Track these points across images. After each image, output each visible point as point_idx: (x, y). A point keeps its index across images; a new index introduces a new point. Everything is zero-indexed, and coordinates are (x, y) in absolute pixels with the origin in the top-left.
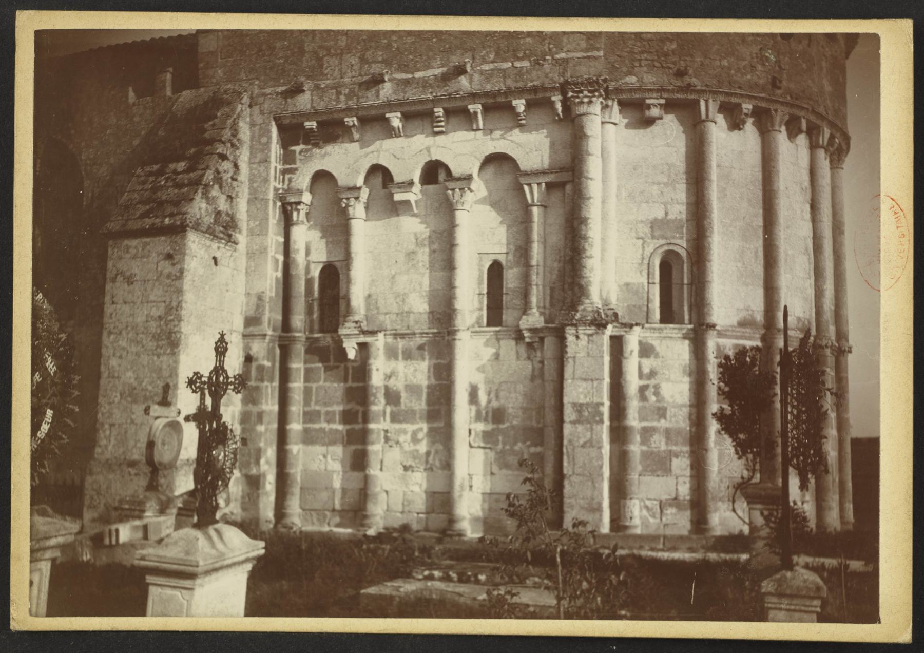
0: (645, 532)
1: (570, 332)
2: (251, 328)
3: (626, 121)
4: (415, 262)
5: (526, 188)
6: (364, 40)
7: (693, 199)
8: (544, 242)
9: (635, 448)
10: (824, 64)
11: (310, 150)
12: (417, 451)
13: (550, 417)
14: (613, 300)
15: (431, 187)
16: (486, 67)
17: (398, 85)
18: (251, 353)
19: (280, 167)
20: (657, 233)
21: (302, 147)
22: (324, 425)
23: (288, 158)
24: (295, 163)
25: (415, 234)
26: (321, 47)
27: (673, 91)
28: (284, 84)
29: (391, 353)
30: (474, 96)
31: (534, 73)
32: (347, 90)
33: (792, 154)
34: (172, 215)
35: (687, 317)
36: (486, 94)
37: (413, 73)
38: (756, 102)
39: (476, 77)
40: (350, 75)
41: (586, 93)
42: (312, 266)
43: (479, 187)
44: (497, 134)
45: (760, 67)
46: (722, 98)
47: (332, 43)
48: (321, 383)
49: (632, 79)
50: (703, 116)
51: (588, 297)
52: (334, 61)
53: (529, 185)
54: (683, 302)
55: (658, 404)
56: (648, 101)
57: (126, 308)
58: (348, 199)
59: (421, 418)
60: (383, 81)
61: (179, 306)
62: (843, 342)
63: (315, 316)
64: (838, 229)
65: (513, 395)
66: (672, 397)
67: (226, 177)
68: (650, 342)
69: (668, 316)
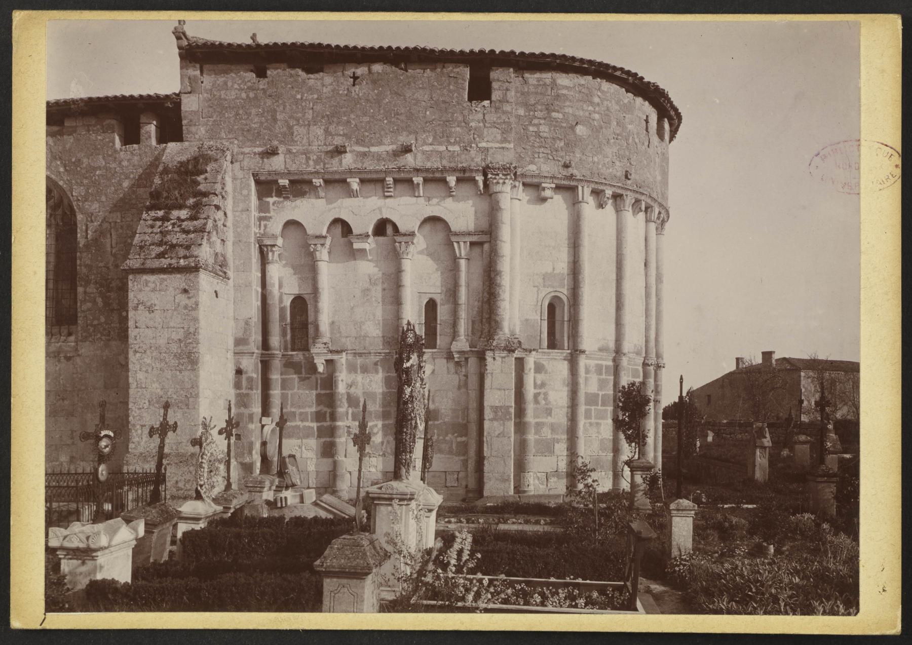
0: (536, 493)
1: (489, 354)
2: (240, 347)
3: (528, 198)
5: (455, 244)
6: (327, 116)
7: (572, 259)
8: (468, 286)
9: (531, 437)
10: (657, 160)
13: (473, 416)
14: (517, 331)
15: (381, 239)
16: (426, 148)
17: (357, 156)
18: (242, 367)
19: (257, 215)
21: (275, 199)
22: (299, 423)
23: (263, 207)
25: (369, 276)
26: (290, 117)
27: (561, 179)
28: (260, 146)
29: (352, 368)
31: (463, 156)
32: (315, 157)
33: (635, 223)
34: (185, 257)
35: (566, 345)
36: (427, 170)
38: (614, 189)
39: (419, 155)
40: (316, 143)
41: (501, 175)
42: (285, 297)
43: (420, 242)
44: (435, 201)
45: (618, 163)
46: (593, 186)
47: (300, 115)
49: (533, 168)
50: (580, 199)
51: (501, 329)
52: (302, 130)
53: (458, 242)
54: (563, 333)
56: (544, 185)
57: (149, 332)
58: (315, 245)
59: (375, 417)
60: (345, 152)
61: (196, 332)
62: (660, 360)
63: (289, 337)
64: (659, 279)
65: (445, 400)
67: (220, 224)
69: (552, 345)
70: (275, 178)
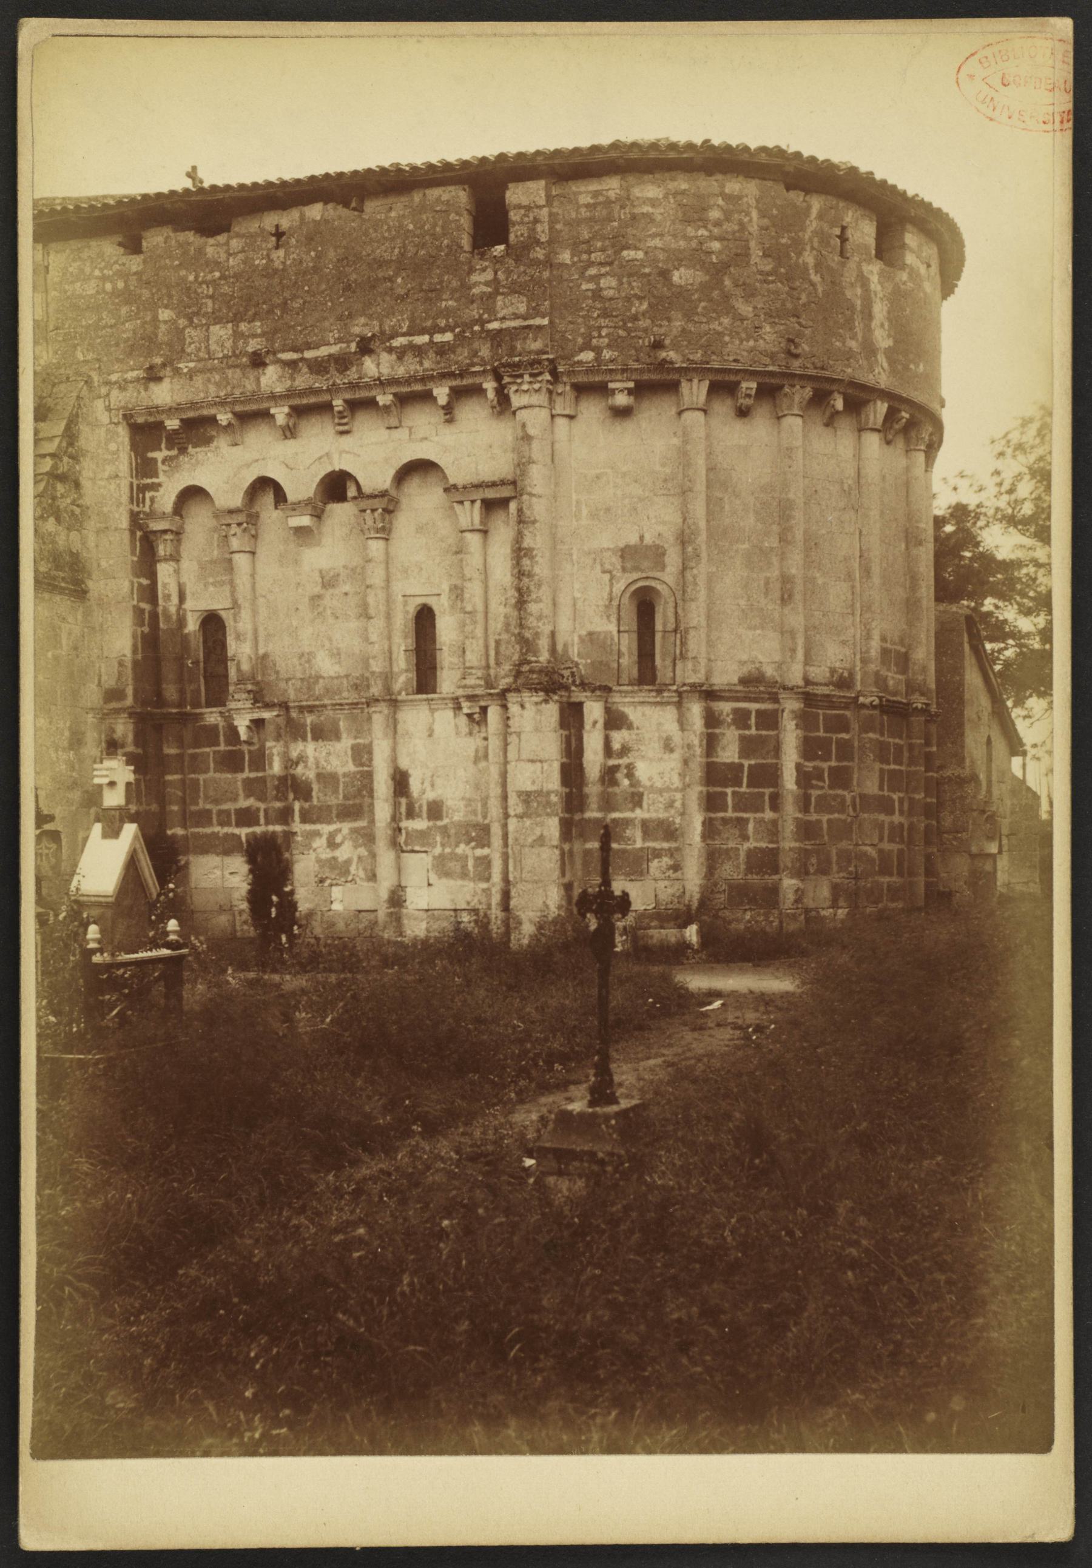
4: (321, 609)
11: (176, 457)
12: (335, 859)
20: (628, 565)
21: (165, 453)
22: (217, 829)
24: (157, 477)
25: (321, 572)
30: (382, 383)
37: (302, 352)
48: (211, 774)
55: (633, 789)
56: (611, 385)
66: (650, 779)
68: (622, 709)
70: (159, 418)
